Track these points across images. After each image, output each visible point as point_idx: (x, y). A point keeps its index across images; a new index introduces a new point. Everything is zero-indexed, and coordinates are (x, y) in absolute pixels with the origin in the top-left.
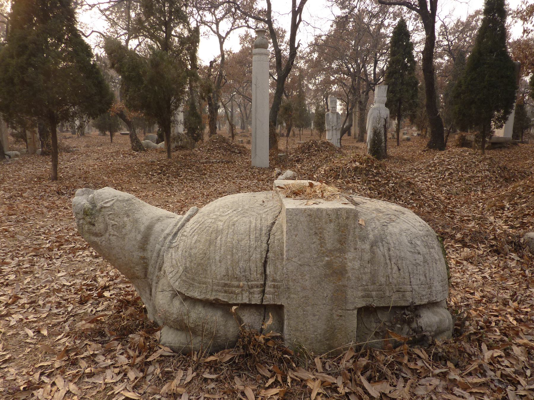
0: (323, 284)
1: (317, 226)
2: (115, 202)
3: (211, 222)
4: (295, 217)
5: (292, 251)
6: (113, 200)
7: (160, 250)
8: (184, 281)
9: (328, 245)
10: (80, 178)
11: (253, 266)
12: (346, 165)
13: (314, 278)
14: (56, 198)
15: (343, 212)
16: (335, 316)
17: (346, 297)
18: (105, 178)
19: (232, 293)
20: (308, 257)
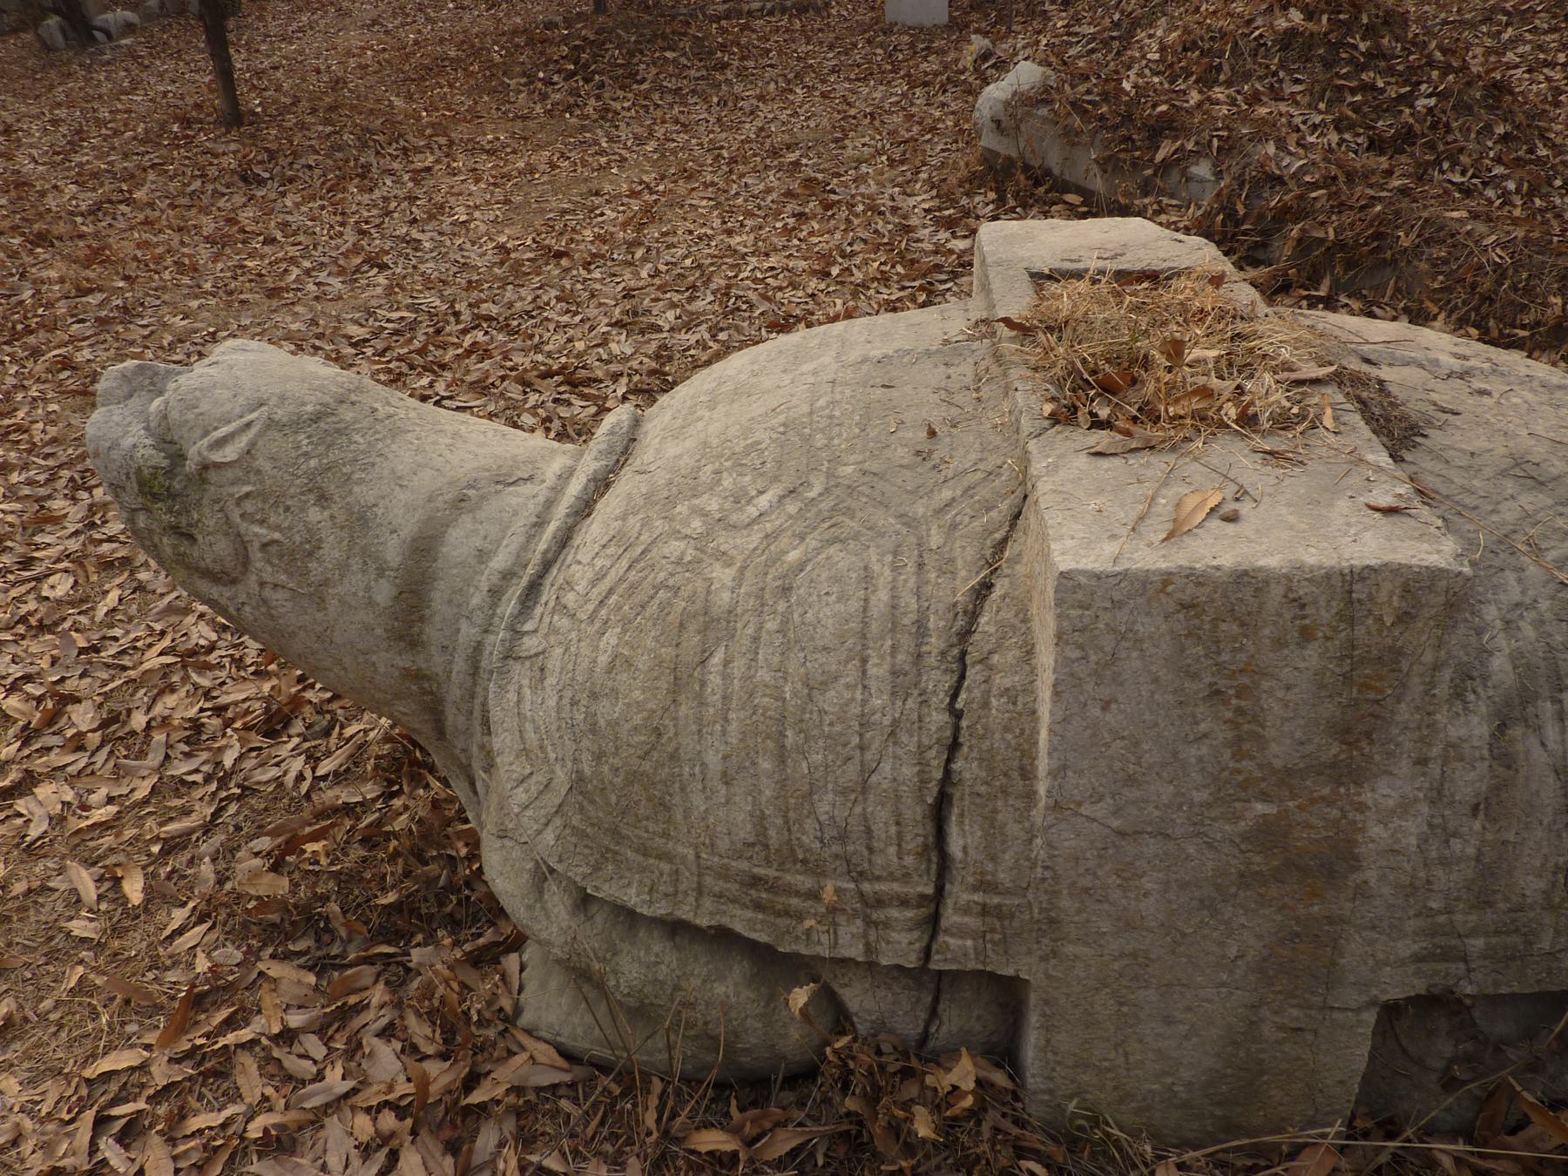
0: (1228, 911)
1: (1225, 657)
2: (260, 435)
3: (679, 561)
4: (1105, 617)
5: (1080, 773)
6: (248, 425)
7: (478, 647)
8: (576, 831)
9: (1274, 748)
10: (314, 111)
11: (881, 817)
12: (1249, 22)
13: (1184, 886)
14: (239, 199)
15: (1387, 586)
16: (1267, 1031)
17: (1334, 964)
18: (398, 102)
19: (786, 913)
20: (1165, 799)
